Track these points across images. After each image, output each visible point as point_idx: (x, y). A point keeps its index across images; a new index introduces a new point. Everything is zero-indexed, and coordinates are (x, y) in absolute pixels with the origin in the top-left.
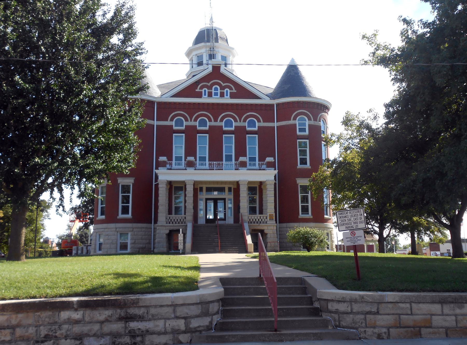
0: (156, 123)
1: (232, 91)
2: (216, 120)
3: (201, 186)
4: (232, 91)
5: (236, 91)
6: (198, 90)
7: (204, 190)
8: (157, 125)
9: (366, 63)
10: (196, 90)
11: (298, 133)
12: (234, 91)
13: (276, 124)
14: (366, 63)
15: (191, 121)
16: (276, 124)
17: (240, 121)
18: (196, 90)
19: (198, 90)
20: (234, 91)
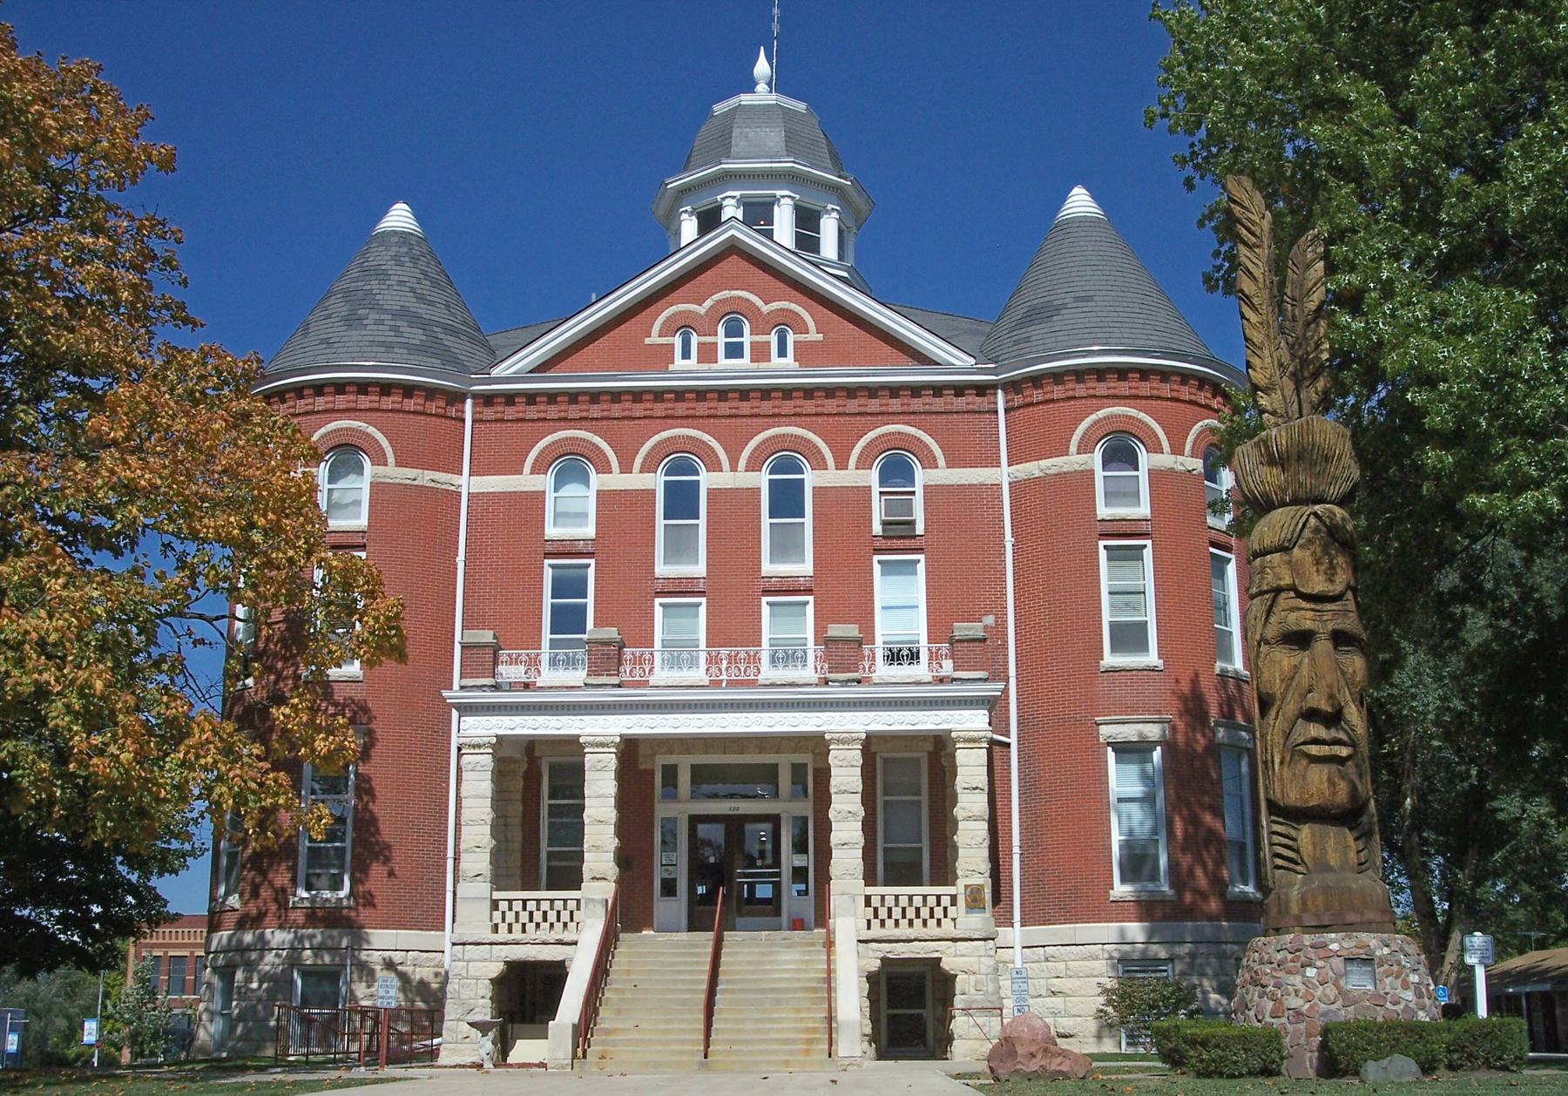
0: (467, 483)
1: (801, 337)
2: (841, 464)
3: (670, 759)
4: (801, 337)
5: (820, 337)
6: (654, 339)
7: (684, 779)
8: (998, 465)
9: (391, 874)
10: (647, 341)
11: (1103, 511)
12: (814, 336)
13: (1003, 474)
14: (391, 874)
15: (734, 468)
16: (1003, 474)
17: (734, 468)
18: (647, 341)
19: (654, 339)
20: (814, 336)
